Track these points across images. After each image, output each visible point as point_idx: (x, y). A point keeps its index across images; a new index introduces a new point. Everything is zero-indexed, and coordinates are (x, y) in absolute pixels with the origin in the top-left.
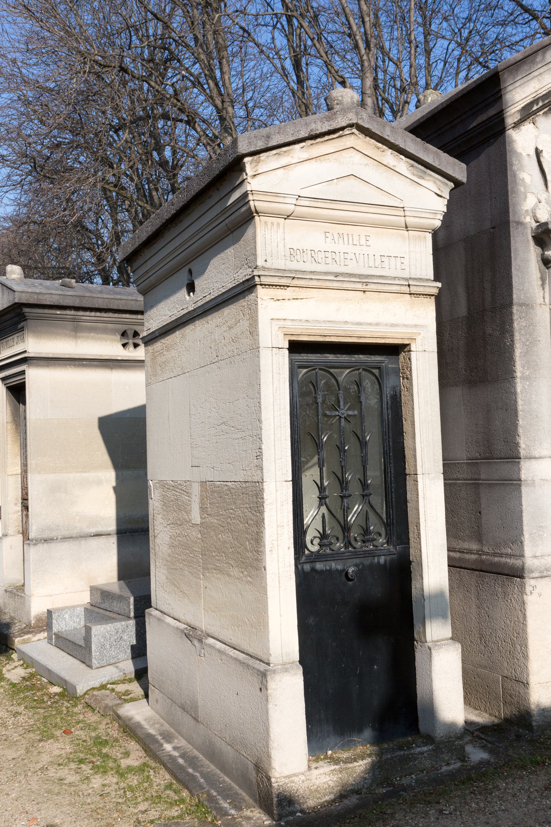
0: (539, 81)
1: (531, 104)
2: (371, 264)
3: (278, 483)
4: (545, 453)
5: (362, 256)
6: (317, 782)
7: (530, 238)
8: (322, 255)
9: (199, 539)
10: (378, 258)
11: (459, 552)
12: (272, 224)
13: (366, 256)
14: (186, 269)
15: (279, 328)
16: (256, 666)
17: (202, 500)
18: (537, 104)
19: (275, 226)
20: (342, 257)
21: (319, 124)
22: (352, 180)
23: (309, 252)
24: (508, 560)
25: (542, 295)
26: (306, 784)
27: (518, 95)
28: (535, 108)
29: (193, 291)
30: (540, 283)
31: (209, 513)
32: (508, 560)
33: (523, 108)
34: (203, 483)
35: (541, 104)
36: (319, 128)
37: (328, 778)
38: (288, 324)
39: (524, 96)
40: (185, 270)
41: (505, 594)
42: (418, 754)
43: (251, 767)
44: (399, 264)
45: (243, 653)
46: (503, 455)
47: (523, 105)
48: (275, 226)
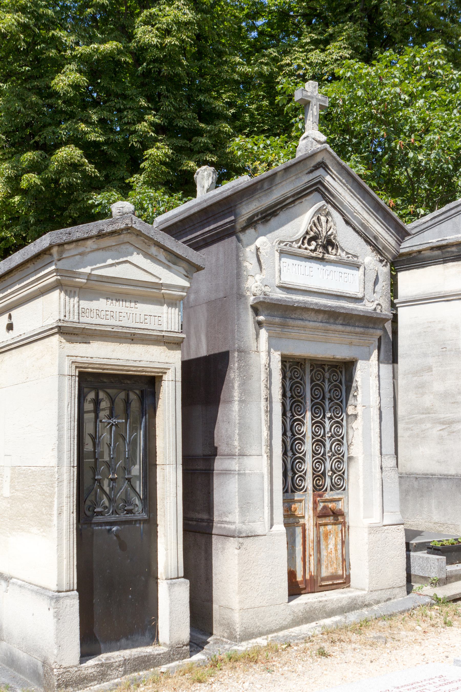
0: (259, 201)
1: (253, 217)
2: (138, 320)
3: (81, 321)
4: (253, 452)
5: (131, 315)
6: (86, 672)
7: (249, 307)
8: (103, 313)
9: (8, 508)
10: (142, 316)
11: (196, 521)
12: (71, 291)
13: (134, 315)
14: (8, 314)
15: (73, 362)
16: (46, 593)
17: (11, 480)
18: (257, 216)
19: (72, 293)
20: (118, 315)
21: (106, 226)
22: (128, 265)
23: (95, 311)
24: (226, 526)
25: (256, 345)
26: (78, 673)
27: (244, 210)
28: (256, 219)
29: (12, 329)
30: (255, 337)
31: (17, 489)
32: (226, 526)
33: (248, 219)
34: (13, 468)
35: (260, 216)
36: (105, 229)
37: (93, 670)
38: (79, 360)
39: (248, 211)
40: (7, 315)
41: (224, 549)
42: (156, 655)
43: (40, 664)
44: (157, 321)
45: (37, 586)
46: (226, 453)
47: (247, 217)
48: (72, 293)
